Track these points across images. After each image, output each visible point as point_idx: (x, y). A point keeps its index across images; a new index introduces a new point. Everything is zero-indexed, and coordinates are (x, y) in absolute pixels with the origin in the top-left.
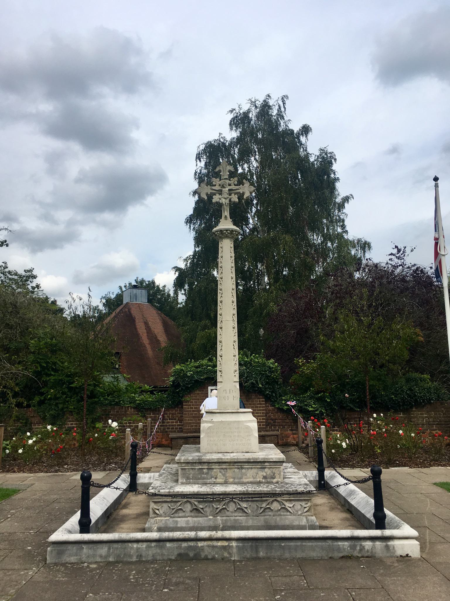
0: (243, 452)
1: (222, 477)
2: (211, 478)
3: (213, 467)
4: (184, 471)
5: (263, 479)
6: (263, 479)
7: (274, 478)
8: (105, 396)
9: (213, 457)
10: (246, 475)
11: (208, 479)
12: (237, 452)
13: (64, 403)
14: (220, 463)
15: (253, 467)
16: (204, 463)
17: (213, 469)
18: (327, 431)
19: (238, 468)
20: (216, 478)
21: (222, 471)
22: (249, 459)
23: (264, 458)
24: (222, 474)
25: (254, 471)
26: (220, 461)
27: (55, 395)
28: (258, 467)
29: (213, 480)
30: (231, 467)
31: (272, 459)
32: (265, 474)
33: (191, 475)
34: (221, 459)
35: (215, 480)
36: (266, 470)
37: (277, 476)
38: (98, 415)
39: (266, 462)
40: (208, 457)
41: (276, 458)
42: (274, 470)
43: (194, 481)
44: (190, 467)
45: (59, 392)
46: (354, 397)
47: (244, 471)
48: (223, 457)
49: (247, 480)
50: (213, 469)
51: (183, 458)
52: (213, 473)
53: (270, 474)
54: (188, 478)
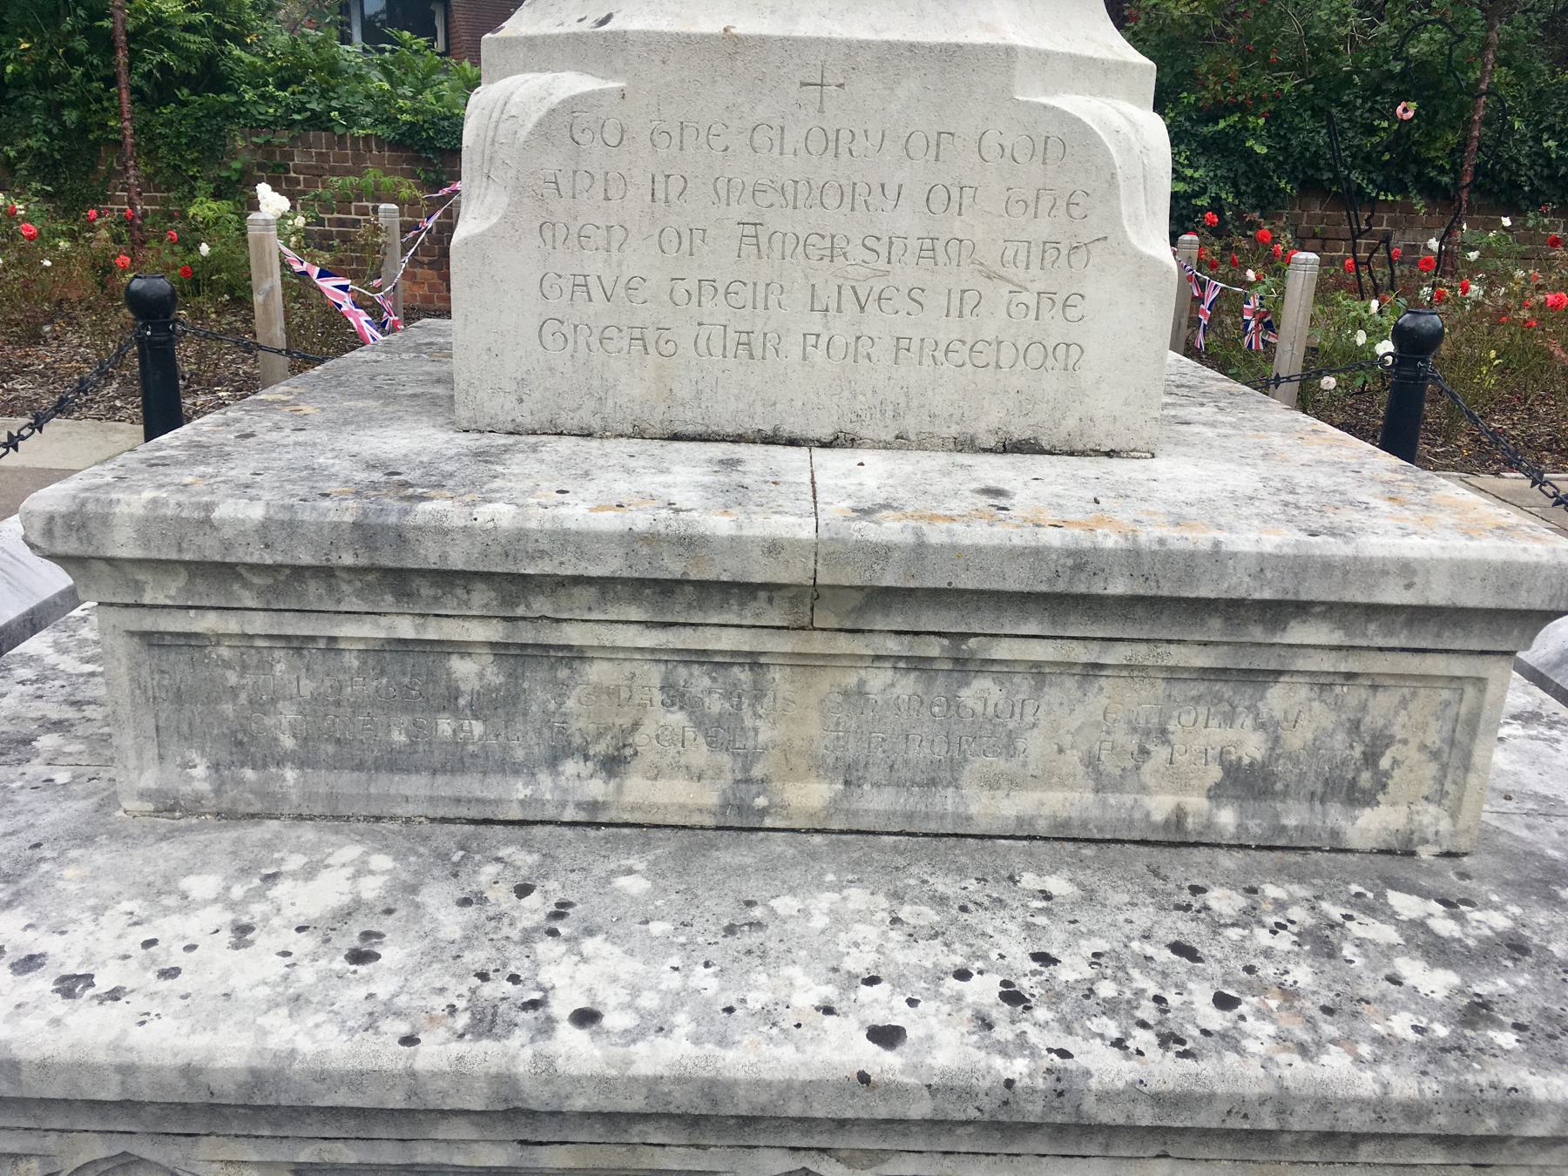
0: (966, 445)
1: (699, 755)
2: (553, 761)
3: (574, 635)
4: (179, 666)
5: (1216, 794)
6: (1216, 794)
7: (1358, 798)
8: (266, 84)
9: (578, 513)
10: (1009, 747)
11: (508, 767)
12: (901, 442)
13: (80, 103)
14: (671, 586)
15: (1116, 655)
16: (446, 579)
17: (575, 656)
18: (1323, 291)
19: (918, 664)
20: (613, 764)
21: (699, 681)
22: (1080, 560)
23: (1300, 565)
24: (700, 720)
25: (1119, 704)
26: (673, 567)
27: (42, 65)
28: (1180, 656)
29: (581, 783)
30: (817, 644)
31: (1407, 570)
32: (1252, 747)
33: (289, 714)
34: (689, 543)
35: (597, 788)
36: (1277, 699)
37: (1409, 767)
38: (236, 165)
39: (1301, 609)
40: (499, 514)
41: (1461, 570)
42: (1383, 702)
43: (323, 781)
44: (259, 624)
45: (52, 53)
46: (1376, 139)
47: (980, 693)
48: (720, 524)
49: (1008, 807)
50: (575, 656)
51: (133, 502)
52: (579, 703)
53: (1314, 749)
54: (244, 746)
